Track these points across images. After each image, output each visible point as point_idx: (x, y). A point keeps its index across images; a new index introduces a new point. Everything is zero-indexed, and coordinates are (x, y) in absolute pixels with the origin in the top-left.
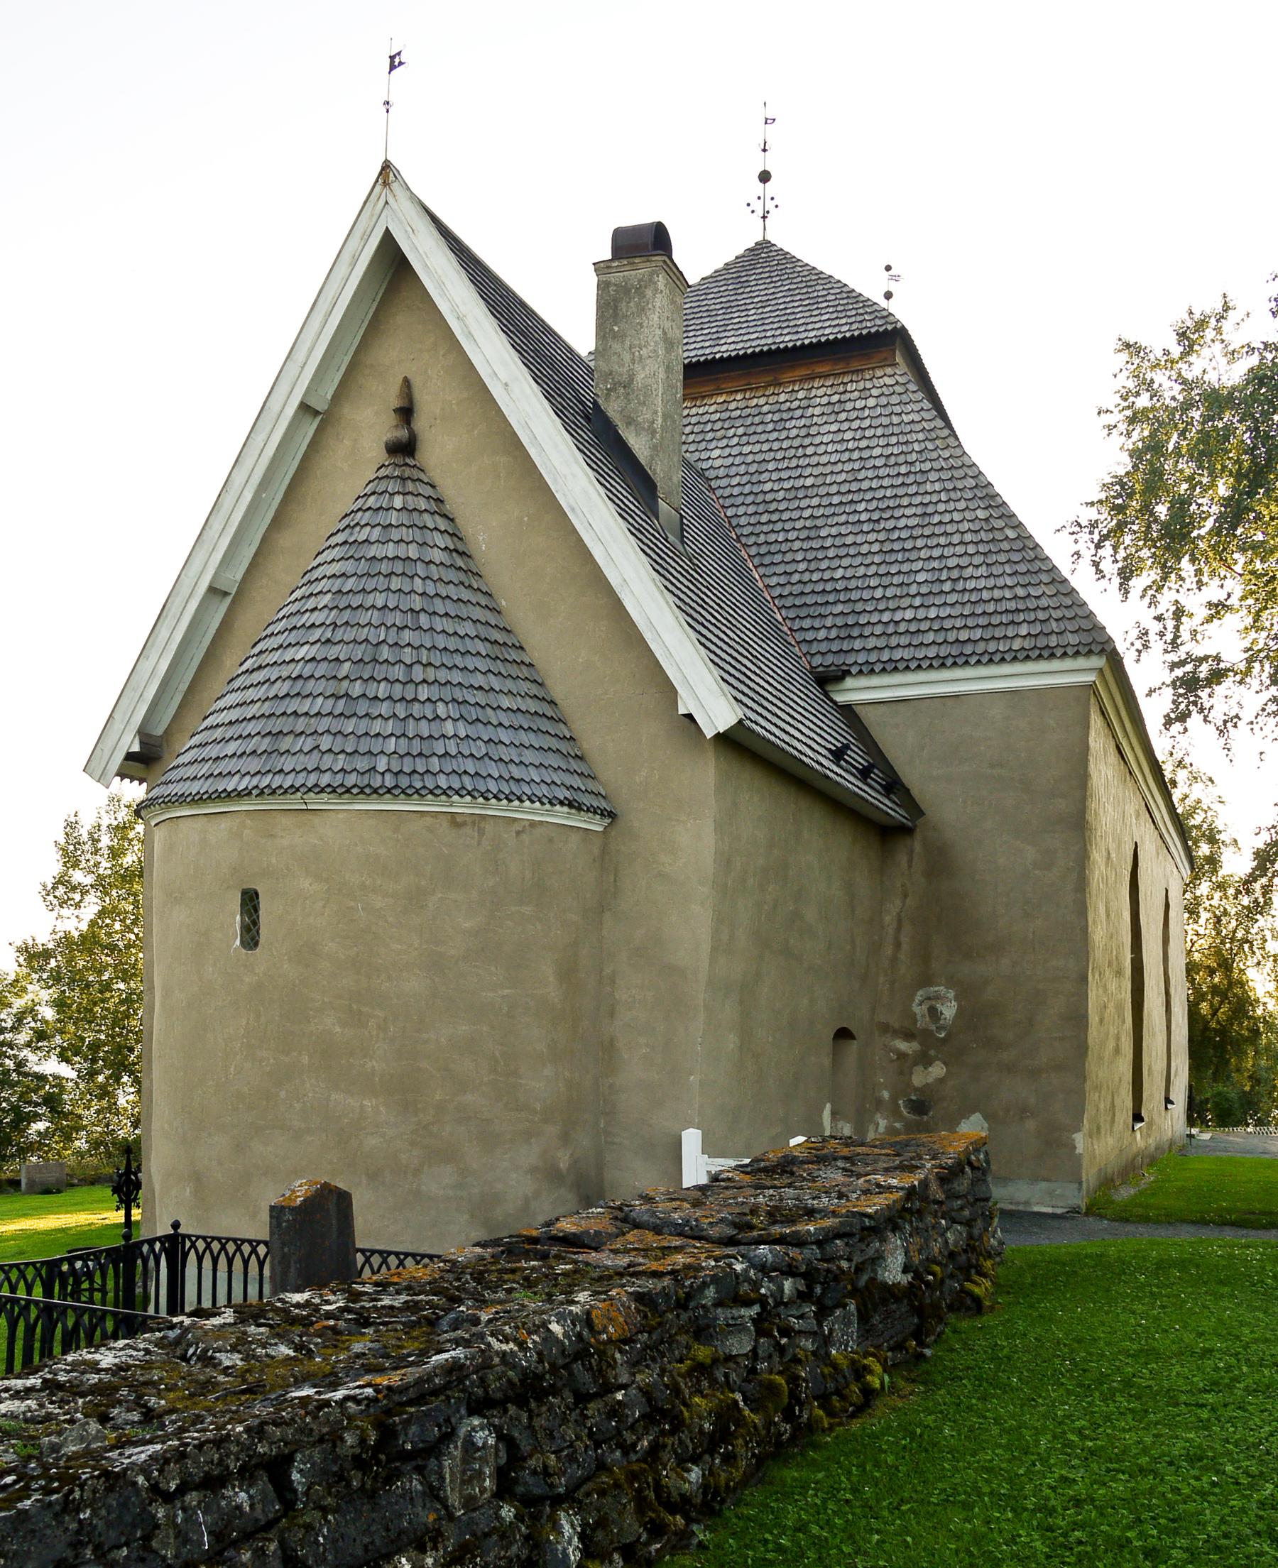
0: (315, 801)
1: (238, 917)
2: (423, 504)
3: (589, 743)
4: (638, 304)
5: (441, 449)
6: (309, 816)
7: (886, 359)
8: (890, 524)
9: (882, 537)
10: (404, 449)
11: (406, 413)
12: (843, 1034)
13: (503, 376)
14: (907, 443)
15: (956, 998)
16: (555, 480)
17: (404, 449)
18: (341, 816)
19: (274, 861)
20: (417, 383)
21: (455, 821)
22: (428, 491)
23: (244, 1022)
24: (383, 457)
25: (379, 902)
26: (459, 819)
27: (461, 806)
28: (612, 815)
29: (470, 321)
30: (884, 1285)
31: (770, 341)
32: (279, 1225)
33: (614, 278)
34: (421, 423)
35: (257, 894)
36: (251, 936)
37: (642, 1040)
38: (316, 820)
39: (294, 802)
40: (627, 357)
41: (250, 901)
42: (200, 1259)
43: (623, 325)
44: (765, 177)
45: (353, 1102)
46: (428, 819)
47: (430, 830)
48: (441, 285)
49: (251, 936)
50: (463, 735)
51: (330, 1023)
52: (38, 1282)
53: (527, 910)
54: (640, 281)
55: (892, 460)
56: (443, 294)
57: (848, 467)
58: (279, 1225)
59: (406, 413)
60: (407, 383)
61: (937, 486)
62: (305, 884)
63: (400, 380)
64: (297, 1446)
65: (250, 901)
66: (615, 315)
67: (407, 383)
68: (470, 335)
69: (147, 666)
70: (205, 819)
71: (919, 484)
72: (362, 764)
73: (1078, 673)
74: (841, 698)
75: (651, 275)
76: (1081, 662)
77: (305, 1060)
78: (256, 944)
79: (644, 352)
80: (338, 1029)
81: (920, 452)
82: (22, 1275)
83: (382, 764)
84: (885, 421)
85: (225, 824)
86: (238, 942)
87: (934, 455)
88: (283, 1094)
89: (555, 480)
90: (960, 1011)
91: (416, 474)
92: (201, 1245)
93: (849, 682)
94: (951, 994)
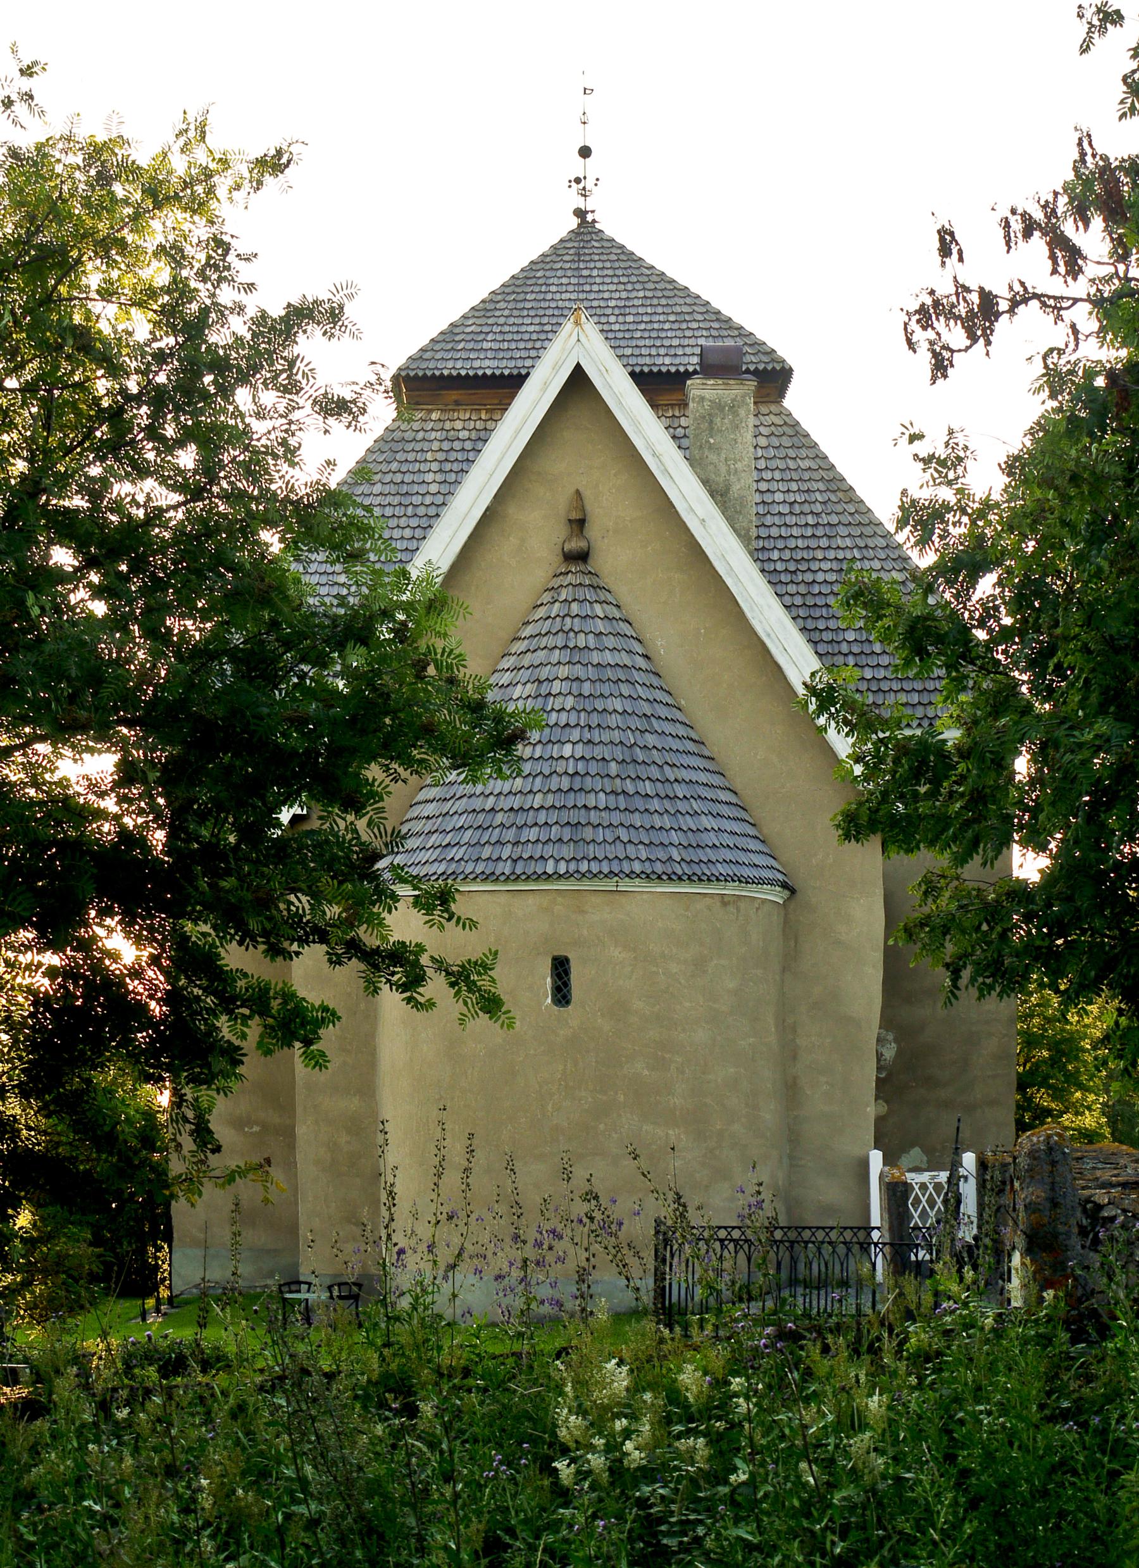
0: (626, 885)
1: (549, 980)
3: (771, 828)
4: (732, 422)
5: (615, 558)
6: (617, 896)
7: (768, 395)
8: (809, 577)
9: (802, 589)
14: (808, 491)
15: (896, 1040)
16: (752, 610)
18: (645, 896)
19: (585, 932)
20: (587, 494)
21: (724, 900)
23: (561, 1067)
25: (674, 968)
26: (726, 899)
27: (731, 890)
28: (793, 891)
31: (648, 360)
32: (895, 1195)
34: (593, 531)
35: (567, 960)
36: (562, 994)
37: (823, 1079)
38: (623, 899)
39: (610, 884)
40: (723, 469)
41: (561, 967)
43: (718, 438)
44: (585, 152)
45: (660, 1132)
46: (708, 900)
47: (709, 908)
49: (562, 994)
50: (602, 806)
51: (639, 1067)
53: (759, 972)
54: (733, 400)
55: (797, 509)
56: (639, 432)
58: (895, 1195)
59: (579, 524)
61: (848, 542)
62: (617, 953)
63: (573, 490)
65: (561, 967)
68: (666, 471)
70: (509, 895)
71: (829, 537)
75: (743, 397)
78: (568, 1002)
79: (739, 465)
80: (646, 1072)
81: (824, 503)
84: (781, 464)
85: (531, 899)
86: (549, 1000)
87: (839, 508)
88: (602, 1127)
89: (752, 610)
90: (900, 1053)
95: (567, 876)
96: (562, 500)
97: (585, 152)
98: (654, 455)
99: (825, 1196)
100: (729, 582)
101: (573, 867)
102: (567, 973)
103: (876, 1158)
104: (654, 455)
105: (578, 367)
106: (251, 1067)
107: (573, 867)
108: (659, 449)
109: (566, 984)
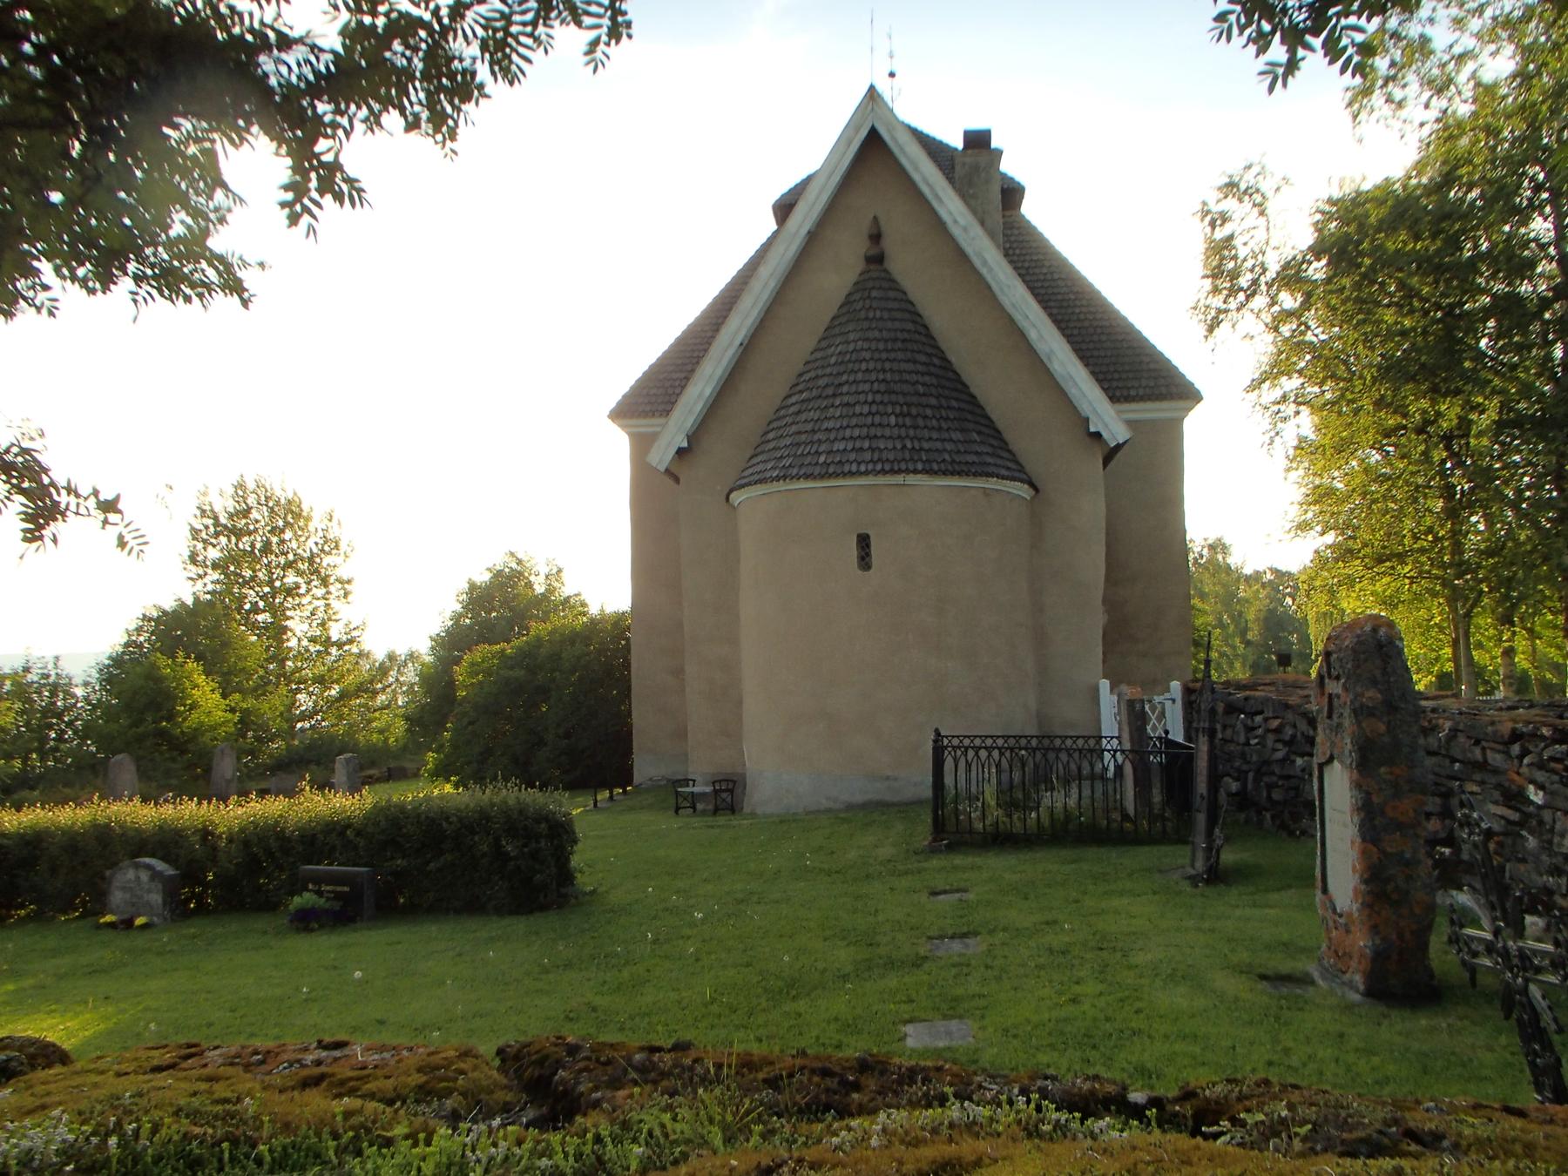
28: (1036, 490)
34: (888, 244)
36: (865, 560)
39: (899, 479)
41: (864, 542)
49: (865, 560)
56: (917, 169)
59: (876, 237)
65: (864, 542)
95: (866, 473)
96: (865, 226)
97: (892, 75)
98: (928, 184)
99: (1067, 716)
100: (984, 271)
101: (870, 467)
102: (868, 546)
103: (1105, 684)
104: (928, 184)
105: (872, 88)
106: (487, 1048)
107: (870, 467)
108: (931, 180)
109: (868, 555)
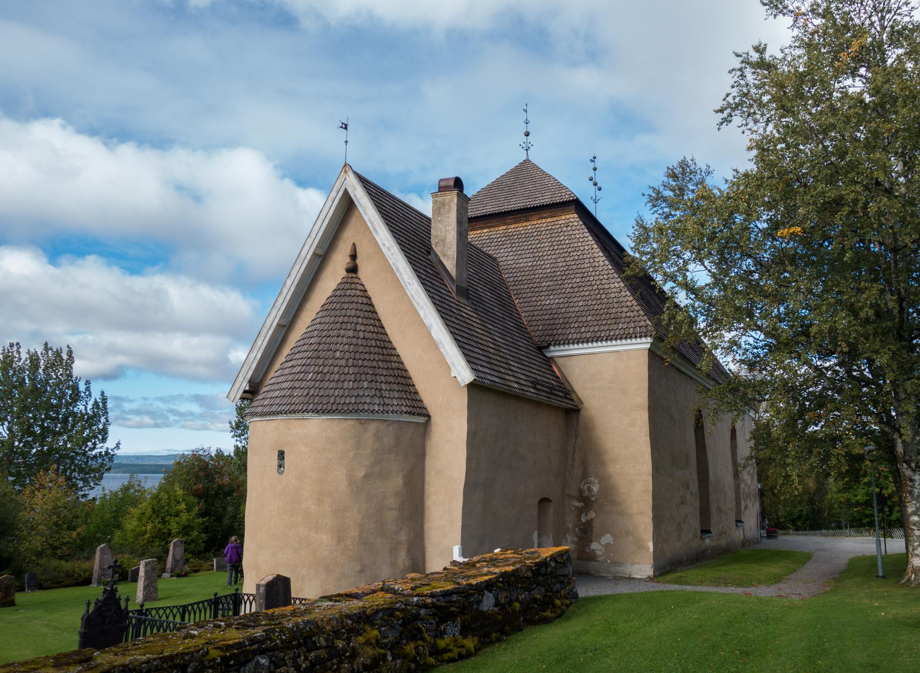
2: (358, 293)
10: (353, 269)
11: (354, 257)
12: (544, 501)
13: (387, 244)
17: (353, 269)
22: (360, 287)
24: (344, 274)
29: (375, 224)
30: (483, 612)
33: (438, 199)
34: (358, 261)
40: (443, 230)
41: (281, 455)
42: (245, 603)
48: (365, 211)
52: (178, 614)
57: (554, 257)
59: (354, 257)
60: (354, 244)
64: (191, 661)
65: (281, 455)
66: (439, 214)
67: (354, 244)
68: (375, 229)
69: (252, 356)
72: (325, 400)
73: (422, 420)
74: (548, 355)
76: (644, 340)
77: (300, 519)
82: (171, 611)
83: (366, 384)
91: (356, 281)
92: (246, 598)
93: (552, 348)
94: (596, 481)
